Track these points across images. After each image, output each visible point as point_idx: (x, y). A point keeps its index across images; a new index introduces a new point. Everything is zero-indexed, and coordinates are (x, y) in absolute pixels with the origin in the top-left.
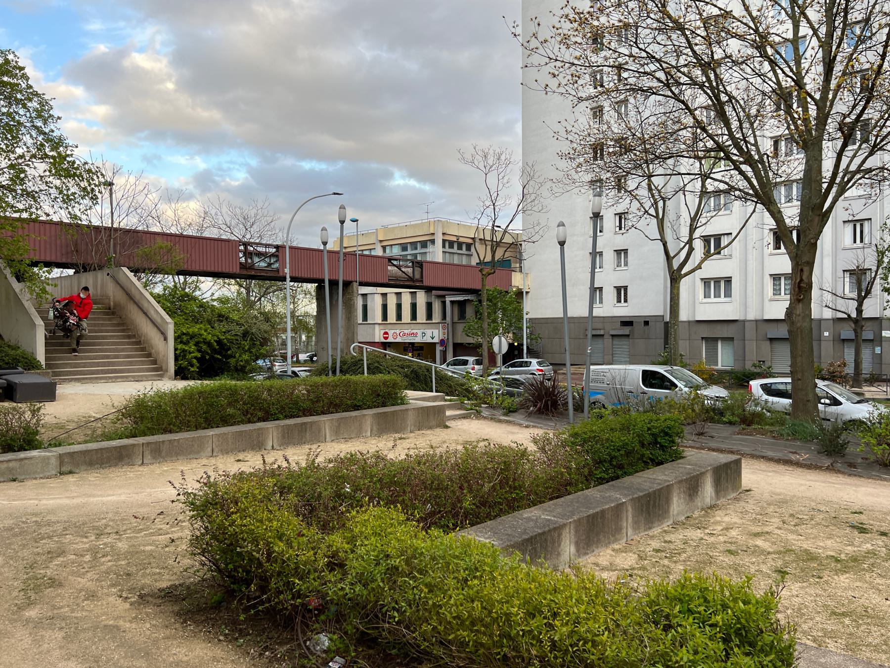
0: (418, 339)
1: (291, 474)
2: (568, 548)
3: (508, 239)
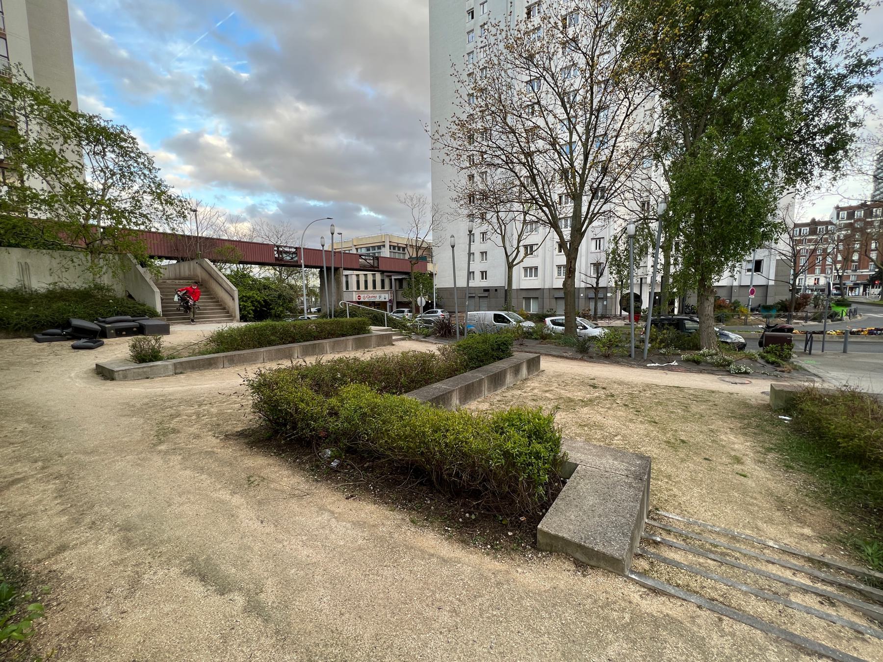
0: (377, 300)
1: (307, 368)
2: (455, 401)
3: (424, 245)
